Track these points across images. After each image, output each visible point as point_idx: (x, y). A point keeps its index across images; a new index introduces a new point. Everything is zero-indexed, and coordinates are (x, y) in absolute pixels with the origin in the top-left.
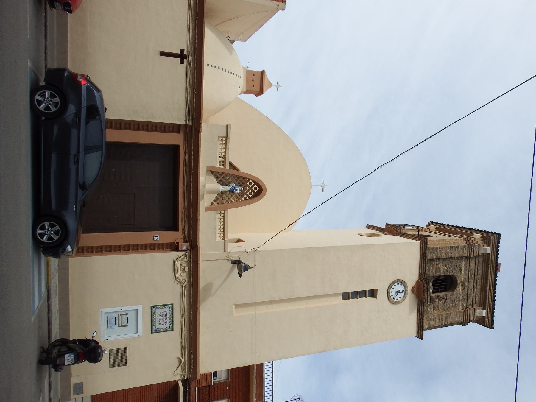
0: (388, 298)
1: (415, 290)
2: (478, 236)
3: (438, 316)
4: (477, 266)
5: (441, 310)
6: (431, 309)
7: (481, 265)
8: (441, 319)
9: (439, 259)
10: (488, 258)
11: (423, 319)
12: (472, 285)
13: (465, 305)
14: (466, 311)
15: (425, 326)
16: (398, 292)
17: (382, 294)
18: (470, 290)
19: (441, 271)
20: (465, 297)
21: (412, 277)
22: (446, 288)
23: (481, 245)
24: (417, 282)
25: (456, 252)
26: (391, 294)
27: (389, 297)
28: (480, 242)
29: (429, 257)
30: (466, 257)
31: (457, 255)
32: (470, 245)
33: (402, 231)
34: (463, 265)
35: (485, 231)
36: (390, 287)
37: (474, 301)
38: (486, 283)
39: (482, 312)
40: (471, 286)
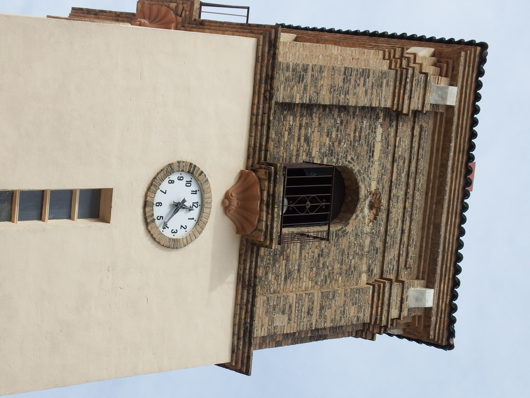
0: (147, 224)
1: (235, 203)
2: (424, 53)
3: (299, 298)
4: (415, 145)
5: (307, 283)
6: (277, 276)
7: (426, 145)
8: (305, 309)
9: (309, 108)
10: (449, 122)
11: (253, 305)
12: (401, 205)
13: (376, 271)
14: (379, 286)
15: (259, 332)
16: (178, 206)
17: (126, 209)
18: (392, 223)
19: (315, 152)
20: (379, 244)
21: (225, 161)
22: (328, 199)
23: (431, 78)
24: (242, 176)
25: (361, 90)
26: (158, 212)
27: (148, 220)
28: (430, 69)
29: (281, 95)
30: (387, 111)
31: (364, 101)
32: (403, 75)
33: (195, 15)
34: (379, 138)
35: (442, 41)
36: (153, 186)
37: (402, 265)
38: (440, 203)
39: (423, 294)
40: (396, 213)
